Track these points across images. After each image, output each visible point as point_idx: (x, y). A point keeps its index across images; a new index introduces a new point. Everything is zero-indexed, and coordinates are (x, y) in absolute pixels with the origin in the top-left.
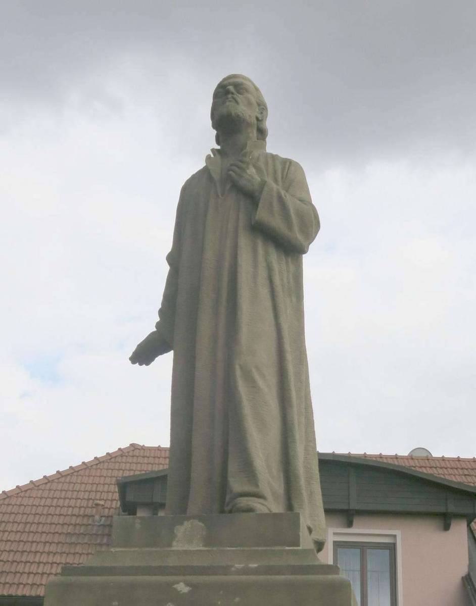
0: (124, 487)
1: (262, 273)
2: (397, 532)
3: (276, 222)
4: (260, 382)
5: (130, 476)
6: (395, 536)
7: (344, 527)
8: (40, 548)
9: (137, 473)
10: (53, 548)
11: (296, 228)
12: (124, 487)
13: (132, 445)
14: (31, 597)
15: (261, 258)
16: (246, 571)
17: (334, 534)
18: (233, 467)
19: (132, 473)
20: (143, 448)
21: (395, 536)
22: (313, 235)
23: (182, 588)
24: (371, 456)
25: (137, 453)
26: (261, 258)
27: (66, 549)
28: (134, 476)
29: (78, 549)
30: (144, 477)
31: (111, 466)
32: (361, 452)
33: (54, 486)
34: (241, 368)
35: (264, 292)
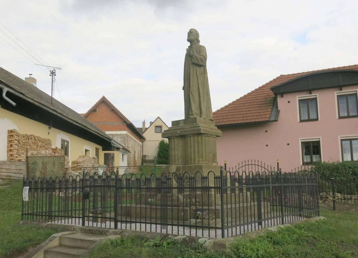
0: (272, 89)
1: (195, 72)
2: (317, 95)
3: (196, 62)
4: (194, 94)
5: (276, 85)
6: (316, 95)
7: (309, 94)
8: (253, 109)
9: (279, 84)
10: (257, 109)
11: (200, 61)
12: (272, 89)
13: (281, 75)
14: (250, 122)
15: (195, 69)
16: (188, 128)
17: (298, 97)
18: (190, 110)
19: (277, 84)
20: (284, 76)
21: (316, 95)
22: (204, 61)
23: (179, 132)
24: (336, 68)
25: (282, 77)
26: (195, 69)
27: (260, 108)
28: (278, 85)
29: (263, 108)
30: (297, 79)
31: (275, 82)
32: (337, 67)
33: (258, 91)
34: (191, 92)
35: (196, 76)
